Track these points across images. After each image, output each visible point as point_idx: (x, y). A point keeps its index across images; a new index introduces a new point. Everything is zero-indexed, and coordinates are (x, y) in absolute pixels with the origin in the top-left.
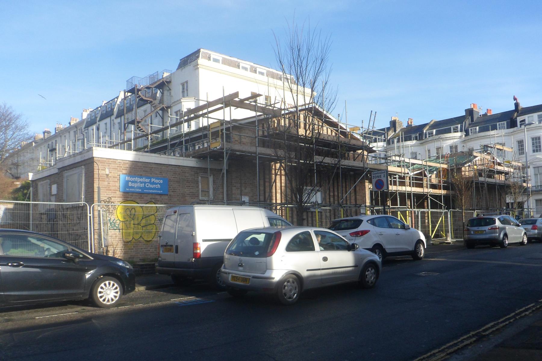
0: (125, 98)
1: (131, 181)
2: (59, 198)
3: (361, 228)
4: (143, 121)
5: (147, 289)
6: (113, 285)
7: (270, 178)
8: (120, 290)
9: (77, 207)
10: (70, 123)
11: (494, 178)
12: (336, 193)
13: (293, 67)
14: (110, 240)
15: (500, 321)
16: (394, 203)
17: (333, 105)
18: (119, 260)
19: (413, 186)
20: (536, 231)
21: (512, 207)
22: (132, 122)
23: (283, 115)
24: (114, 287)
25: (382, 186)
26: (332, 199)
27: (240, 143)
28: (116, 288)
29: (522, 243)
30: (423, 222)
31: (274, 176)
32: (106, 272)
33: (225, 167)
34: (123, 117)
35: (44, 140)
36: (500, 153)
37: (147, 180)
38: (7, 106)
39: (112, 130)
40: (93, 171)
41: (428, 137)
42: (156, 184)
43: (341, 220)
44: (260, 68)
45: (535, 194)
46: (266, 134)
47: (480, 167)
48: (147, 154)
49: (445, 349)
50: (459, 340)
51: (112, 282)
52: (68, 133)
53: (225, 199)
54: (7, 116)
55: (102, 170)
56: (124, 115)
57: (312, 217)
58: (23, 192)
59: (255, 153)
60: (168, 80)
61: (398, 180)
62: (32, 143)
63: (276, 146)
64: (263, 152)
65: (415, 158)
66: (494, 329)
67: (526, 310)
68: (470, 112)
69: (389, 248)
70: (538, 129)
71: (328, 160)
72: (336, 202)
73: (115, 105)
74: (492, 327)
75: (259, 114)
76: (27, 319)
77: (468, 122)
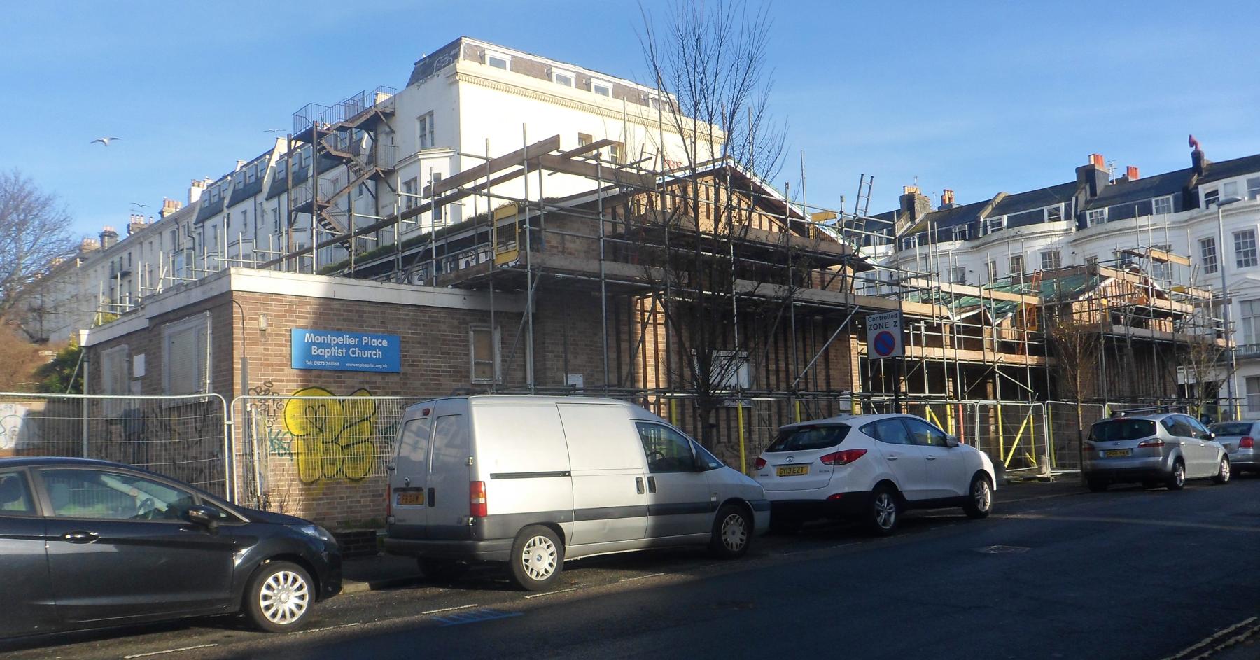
0: (290, 152)
1: (315, 344)
2: (151, 383)
3: (846, 445)
4: (332, 205)
5: (373, 587)
6: (295, 580)
7: (632, 333)
8: (309, 589)
9: (195, 406)
10: (161, 213)
11: (1147, 326)
12: (782, 365)
13: (684, 77)
14: (271, 479)
16: (916, 385)
18: (306, 523)
19: (960, 348)
20: (1251, 451)
21: (1192, 396)
22: (308, 208)
23: (660, 185)
24: (297, 585)
26: (773, 378)
27: (563, 252)
28: (301, 587)
29: (1218, 479)
30: (985, 430)
31: (639, 326)
33: (530, 307)
34: (284, 197)
35: (103, 253)
36: (1161, 267)
38: (22, 178)
39: (259, 226)
40: (232, 323)
41: (989, 232)
42: (372, 349)
44: (598, 80)
46: (621, 229)
47: (1117, 302)
48: (353, 281)
51: (291, 575)
52: (157, 236)
54: (22, 201)
55: (251, 319)
56: (287, 190)
58: (60, 373)
59: (599, 275)
60: (388, 111)
61: (924, 333)
62: (75, 259)
63: (649, 259)
65: (962, 282)
67: (1238, 632)
68: (1088, 174)
69: (912, 489)
72: (783, 386)
73: (265, 169)
75: (603, 185)
77: (1083, 196)
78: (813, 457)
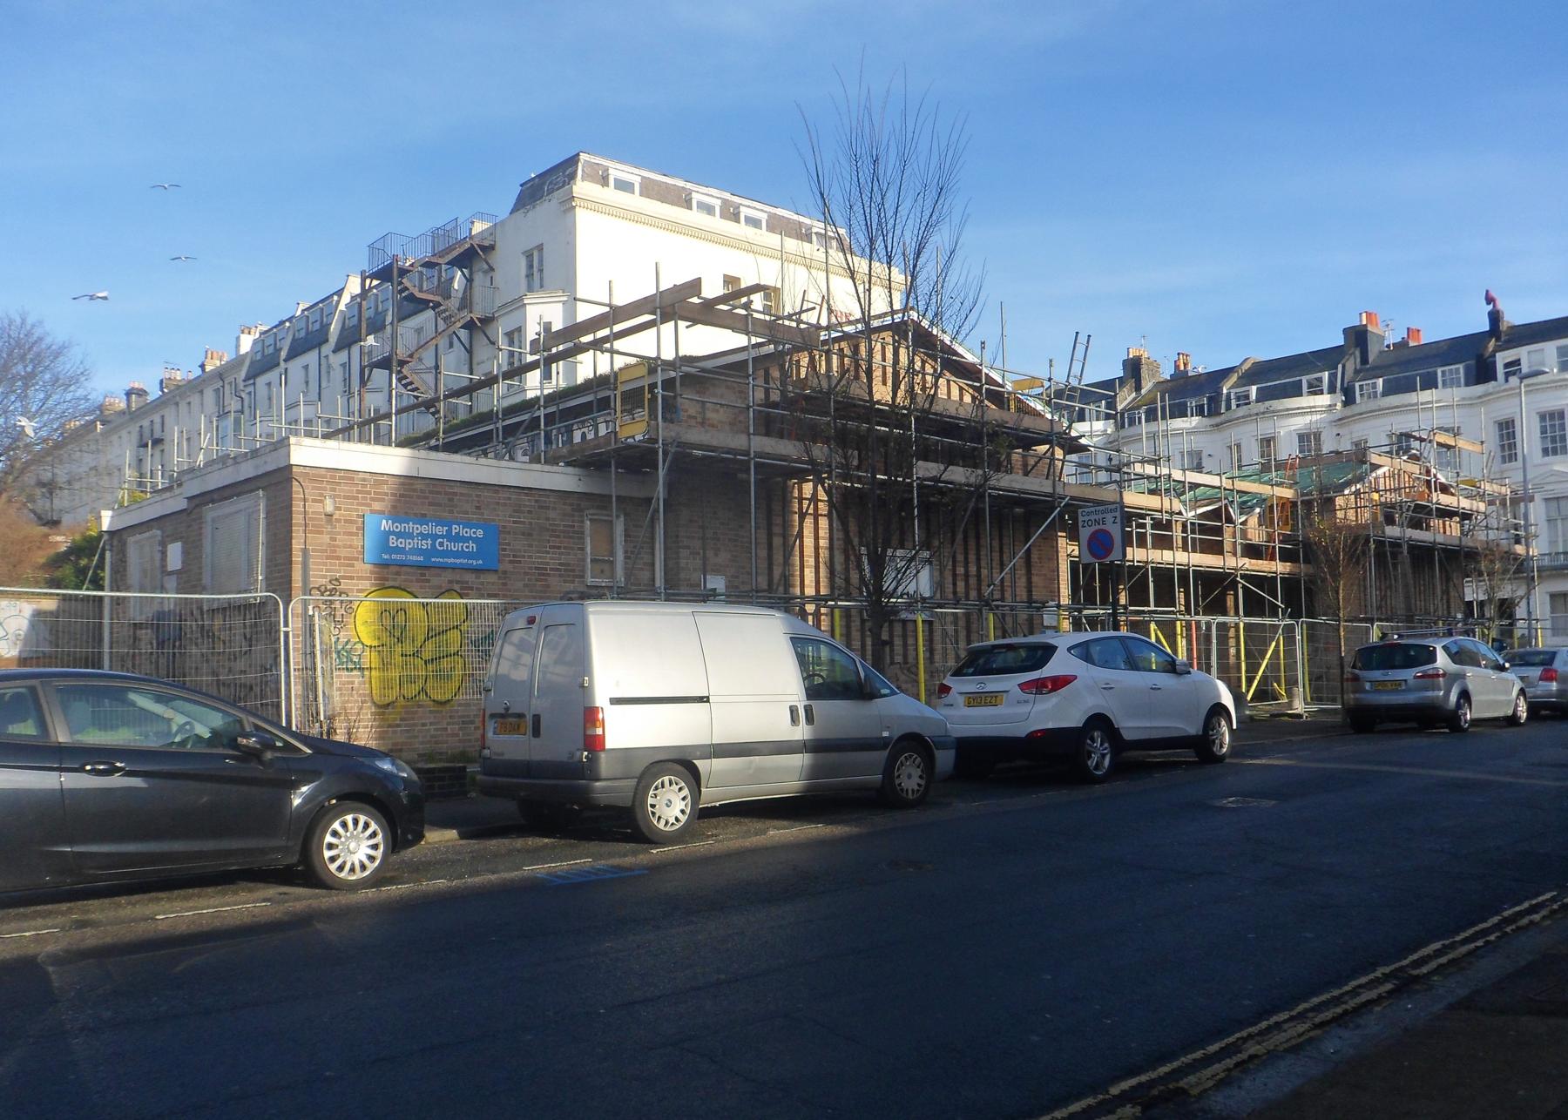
0: (364, 293)
1: (393, 533)
3: (1051, 669)
5: (463, 836)
6: (366, 826)
7: (786, 525)
9: (243, 608)
10: (202, 366)
11: (1428, 528)
12: (973, 569)
13: (858, 208)
15: (1458, 938)
16: (1139, 597)
17: (973, 317)
19: (1194, 551)
20: (1554, 686)
21: (1482, 615)
22: (385, 364)
23: (825, 342)
25: (1108, 549)
26: (961, 585)
27: (703, 424)
28: (374, 835)
29: (1512, 720)
30: (1223, 654)
32: (347, 789)
35: (129, 415)
36: (1450, 455)
37: (440, 530)
39: (324, 385)
40: (291, 506)
43: (994, 647)
45: (1550, 577)
46: (775, 396)
47: (1391, 497)
49: (1306, 1011)
50: (1347, 988)
51: (362, 819)
53: (659, 582)
54: (30, 349)
57: (904, 637)
58: (76, 563)
59: (747, 453)
60: (486, 243)
61: (1150, 531)
62: (93, 422)
63: (812, 434)
64: (768, 450)
65: (1199, 468)
66: (1443, 960)
67: (1533, 910)
68: (1358, 336)
69: (1131, 726)
70: (1549, 385)
71: (958, 474)
72: (973, 594)
73: (332, 314)
74: (1439, 953)
76: (134, 920)
77: (1351, 364)
78: (1010, 683)
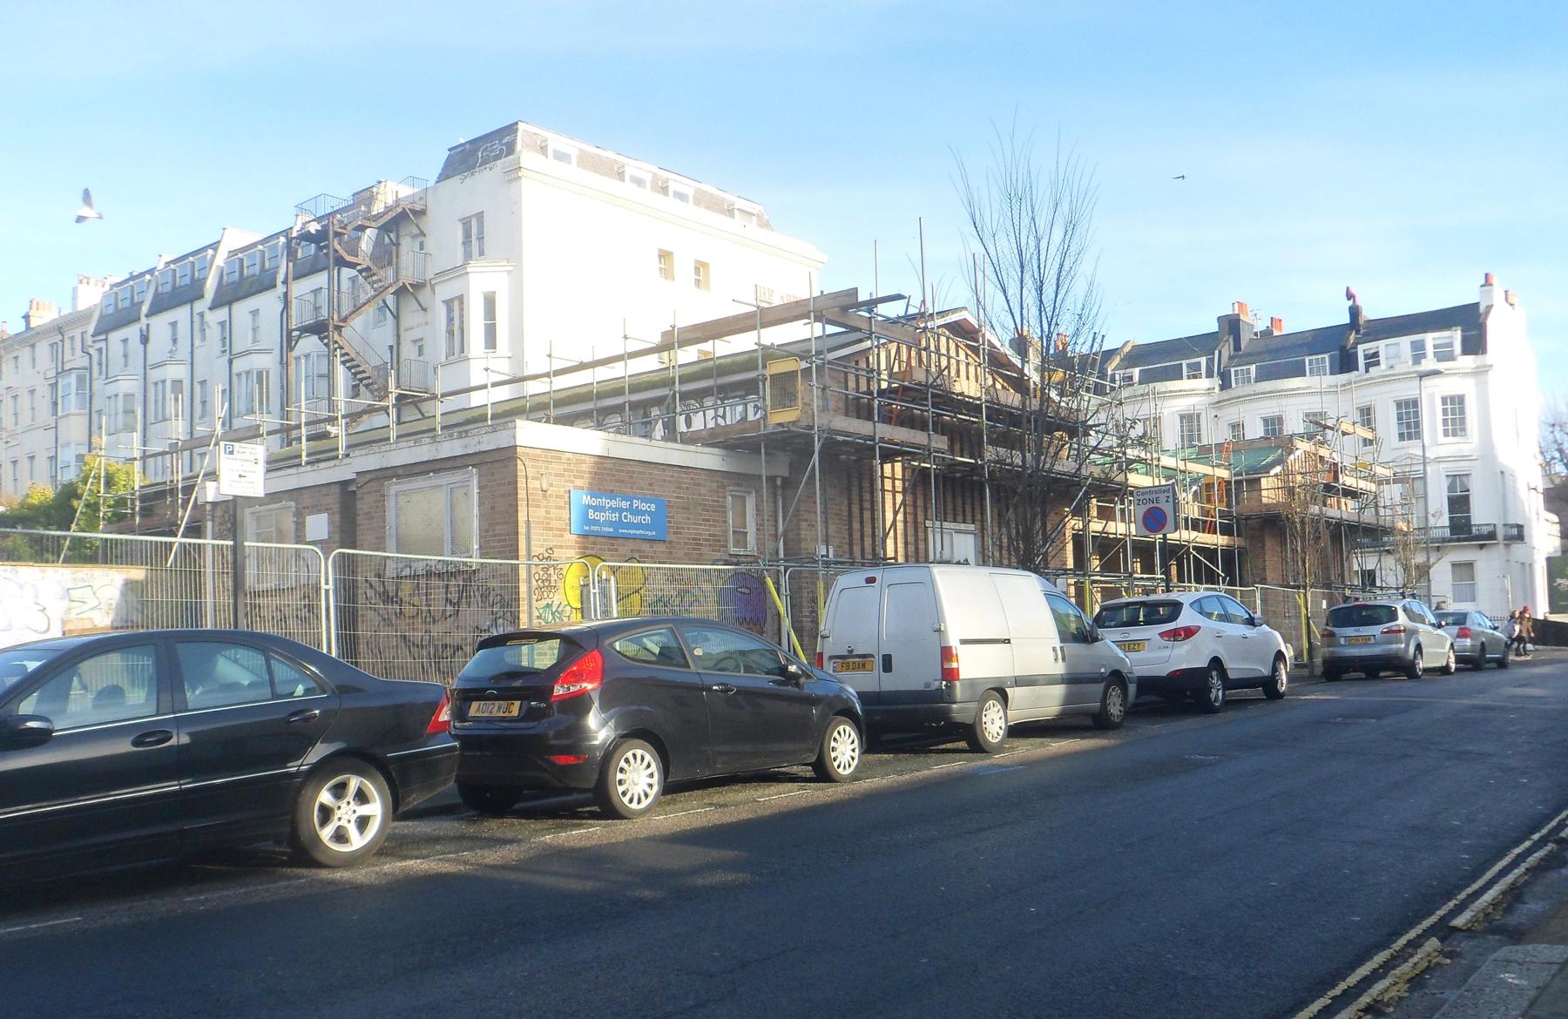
10: (27, 317)
16: (1110, 566)
20: (1468, 642)
29: (1444, 670)
37: (625, 504)
39: (197, 342)
42: (641, 513)
52: (27, 350)
59: (872, 438)
60: (418, 208)
68: (1231, 325)
78: (1152, 632)
